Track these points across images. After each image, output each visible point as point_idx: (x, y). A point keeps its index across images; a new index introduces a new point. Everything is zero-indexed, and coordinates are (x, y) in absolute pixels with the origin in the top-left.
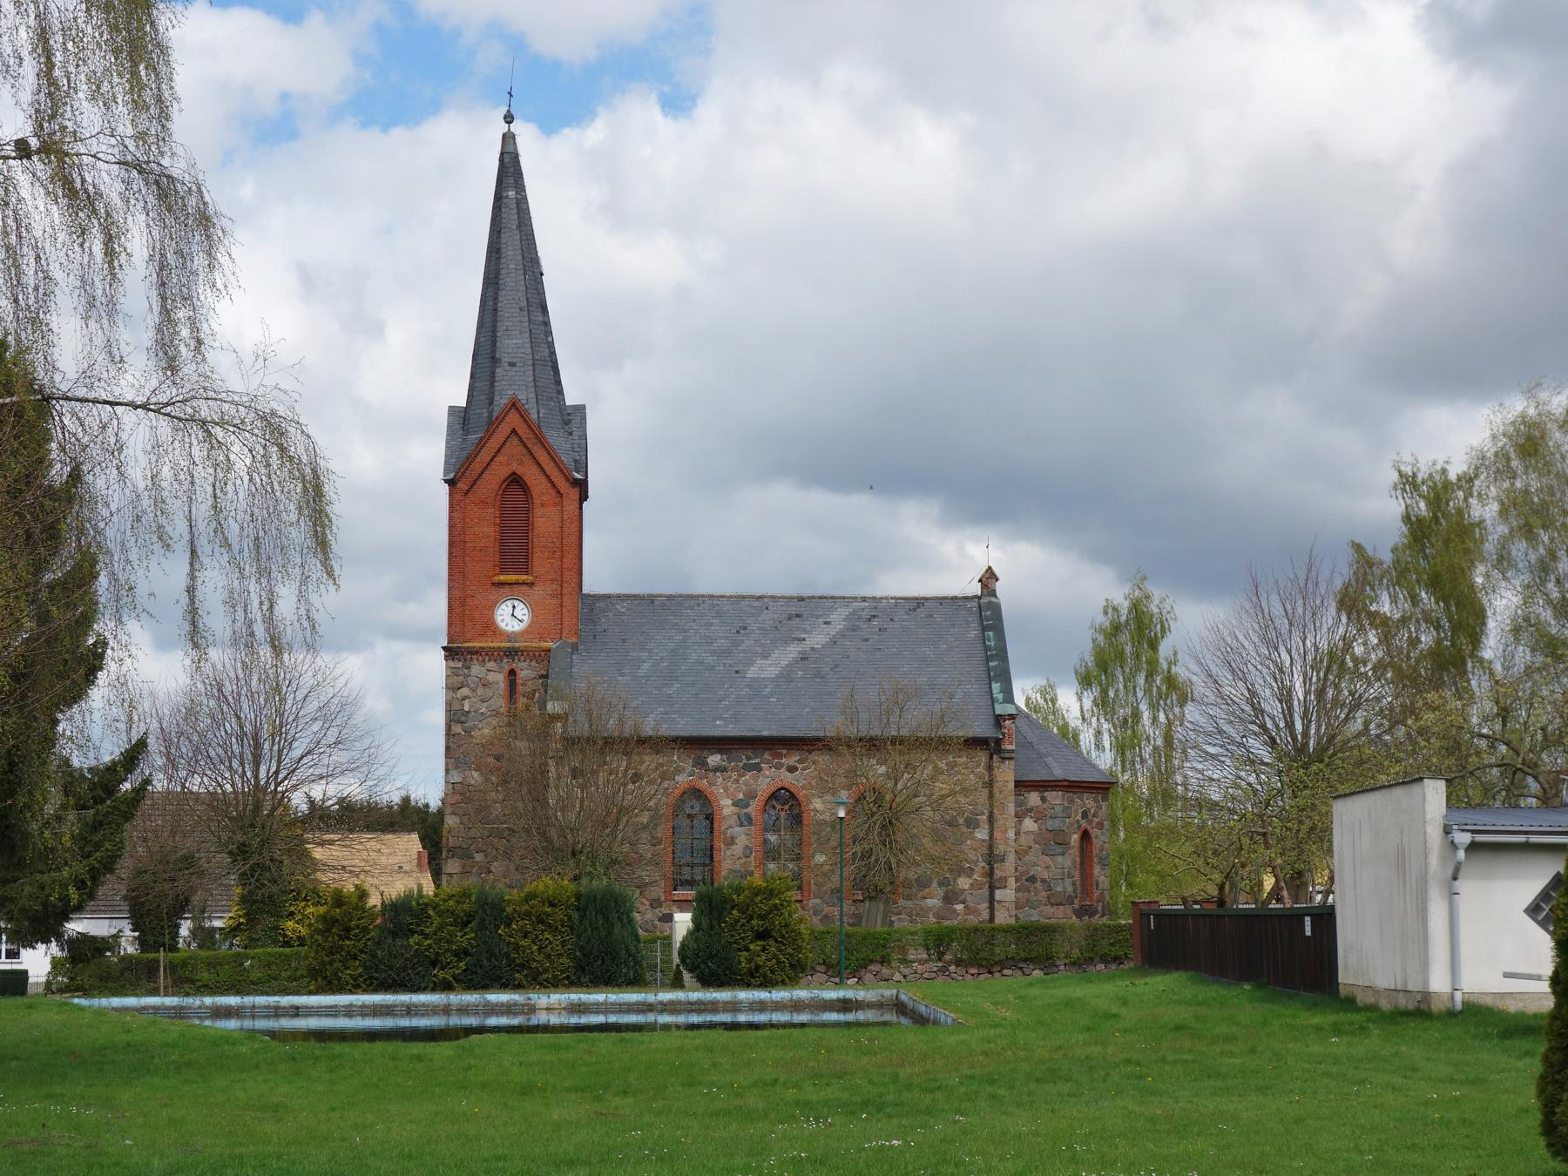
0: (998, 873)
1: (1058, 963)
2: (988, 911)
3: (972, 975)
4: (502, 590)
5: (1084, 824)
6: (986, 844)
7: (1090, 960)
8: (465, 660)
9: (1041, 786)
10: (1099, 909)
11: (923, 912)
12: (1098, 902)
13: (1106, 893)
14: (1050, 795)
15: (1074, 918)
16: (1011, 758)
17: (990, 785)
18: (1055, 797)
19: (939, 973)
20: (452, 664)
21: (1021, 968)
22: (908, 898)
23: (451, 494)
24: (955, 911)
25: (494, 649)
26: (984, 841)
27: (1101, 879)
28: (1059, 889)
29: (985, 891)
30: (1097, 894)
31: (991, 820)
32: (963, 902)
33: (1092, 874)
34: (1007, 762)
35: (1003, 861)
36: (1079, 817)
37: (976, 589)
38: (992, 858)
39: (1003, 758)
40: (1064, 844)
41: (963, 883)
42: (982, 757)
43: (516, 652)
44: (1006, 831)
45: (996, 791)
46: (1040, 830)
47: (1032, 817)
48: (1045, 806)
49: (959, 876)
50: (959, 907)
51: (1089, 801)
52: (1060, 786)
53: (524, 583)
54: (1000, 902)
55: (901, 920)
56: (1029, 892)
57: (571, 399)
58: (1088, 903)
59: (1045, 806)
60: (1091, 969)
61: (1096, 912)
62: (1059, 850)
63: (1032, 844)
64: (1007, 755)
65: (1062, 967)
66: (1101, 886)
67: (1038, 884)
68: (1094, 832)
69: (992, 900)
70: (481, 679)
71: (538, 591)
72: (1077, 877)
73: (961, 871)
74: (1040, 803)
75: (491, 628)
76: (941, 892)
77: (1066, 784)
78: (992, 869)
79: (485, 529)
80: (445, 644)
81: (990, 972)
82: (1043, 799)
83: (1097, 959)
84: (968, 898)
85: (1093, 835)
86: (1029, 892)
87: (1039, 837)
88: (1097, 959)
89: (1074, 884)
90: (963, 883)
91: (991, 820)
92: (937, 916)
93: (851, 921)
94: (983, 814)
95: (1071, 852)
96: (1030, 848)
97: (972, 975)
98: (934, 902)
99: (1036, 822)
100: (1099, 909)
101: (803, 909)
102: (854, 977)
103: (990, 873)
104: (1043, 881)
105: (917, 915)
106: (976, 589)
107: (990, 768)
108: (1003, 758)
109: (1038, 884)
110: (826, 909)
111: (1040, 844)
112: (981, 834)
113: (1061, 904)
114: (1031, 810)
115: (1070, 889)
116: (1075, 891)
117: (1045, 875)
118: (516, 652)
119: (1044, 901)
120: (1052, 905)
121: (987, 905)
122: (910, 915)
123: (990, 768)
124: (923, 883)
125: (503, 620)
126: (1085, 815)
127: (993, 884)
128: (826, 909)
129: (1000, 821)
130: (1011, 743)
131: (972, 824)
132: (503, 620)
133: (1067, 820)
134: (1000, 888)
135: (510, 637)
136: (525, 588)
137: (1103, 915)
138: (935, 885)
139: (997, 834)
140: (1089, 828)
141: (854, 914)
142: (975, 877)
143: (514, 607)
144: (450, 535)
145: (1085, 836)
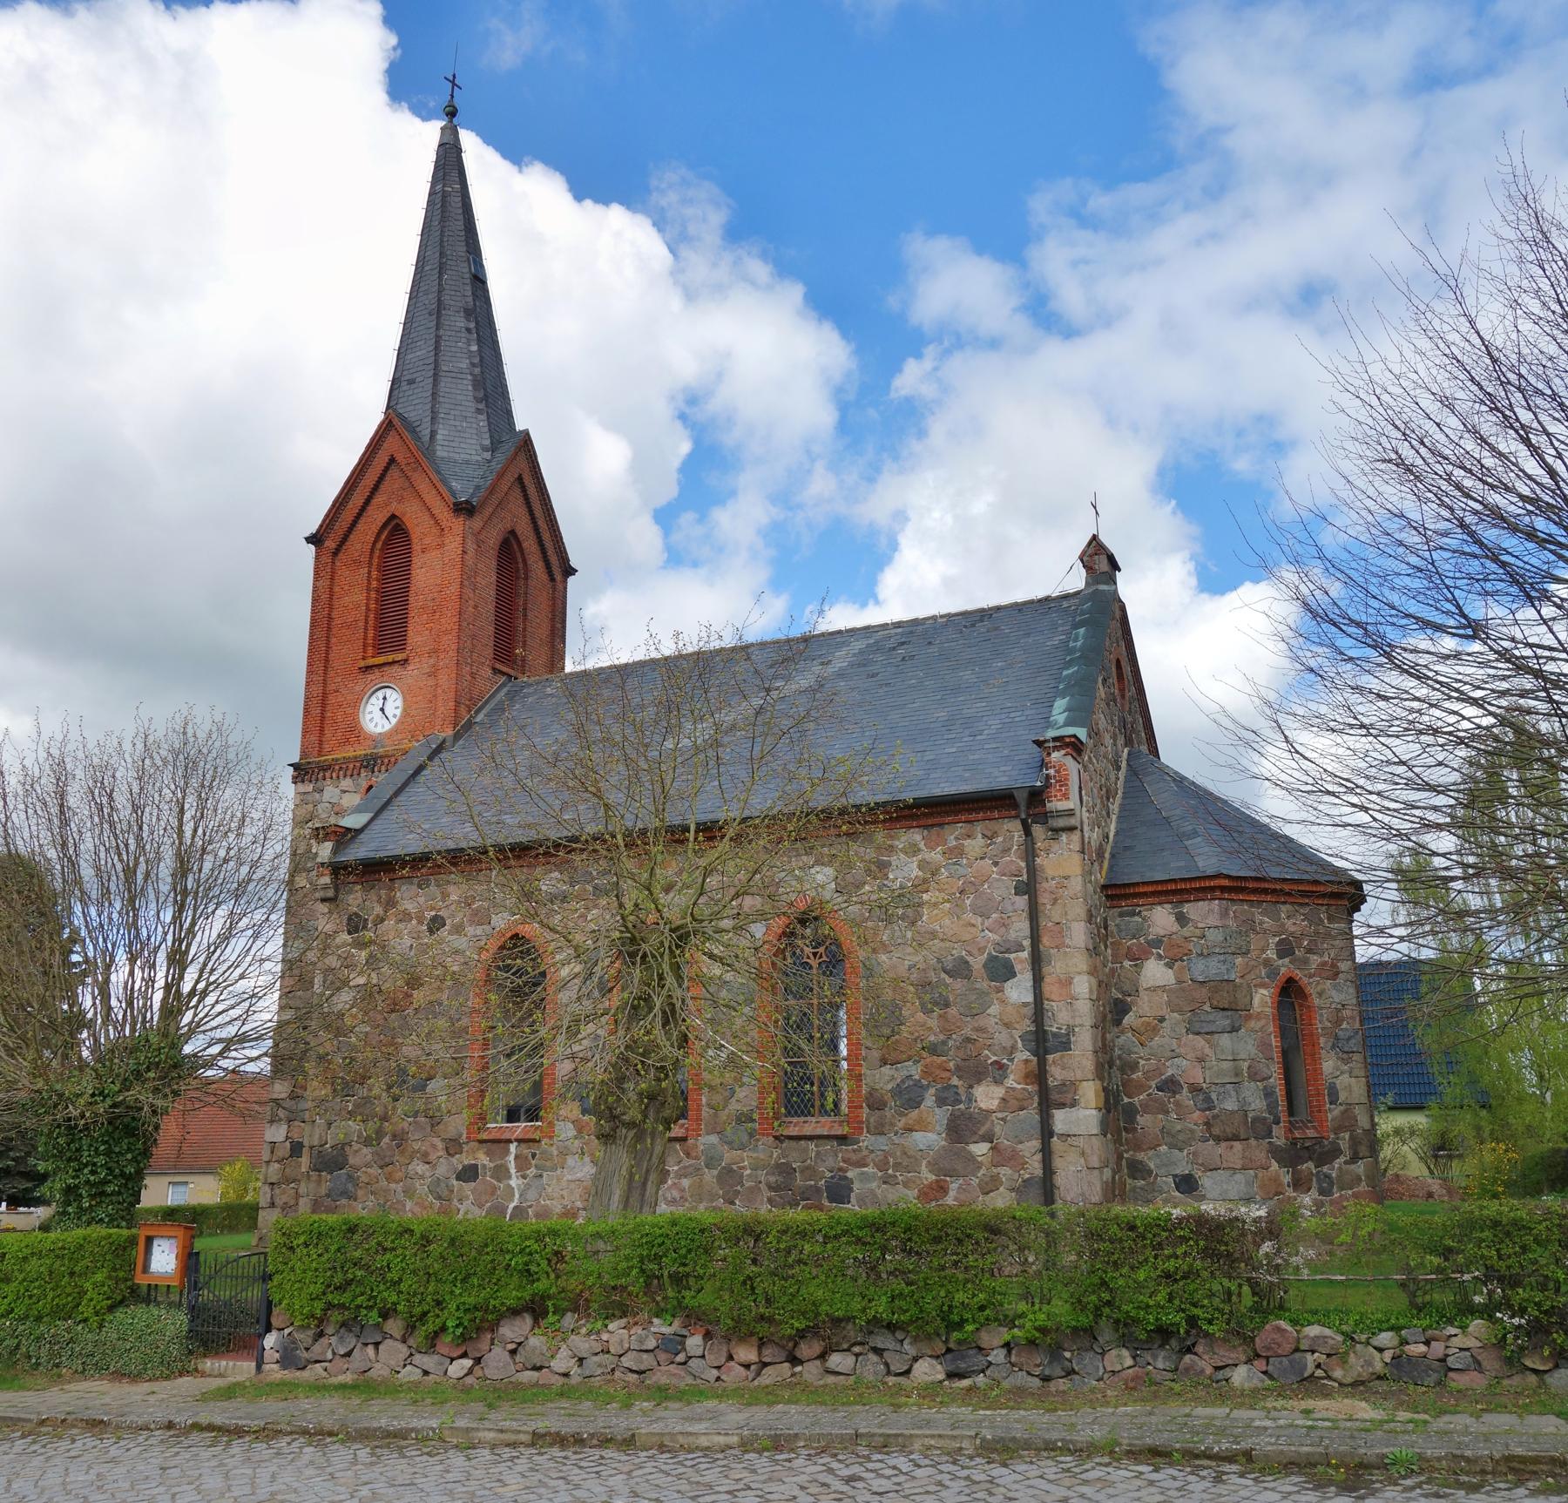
0: (1056, 1074)
1: (986, 1339)
2: (1039, 1156)
3: (747, 1366)
4: (371, 677)
5: (1285, 967)
6: (1029, 1011)
7: (1086, 1335)
8: (317, 780)
9: (1174, 892)
10: (1344, 1145)
11: (908, 1162)
12: (1337, 1130)
13: (1357, 1110)
14: (1195, 910)
15: (1275, 1165)
16: (1071, 829)
17: (1029, 887)
18: (1204, 913)
19: (662, 1357)
20: (303, 788)
21: (878, 1351)
22: (879, 1131)
23: (317, 558)
24: (971, 1158)
25: (347, 760)
26: (1025, 1005)
27: (1343, 1081)
28: (1230, 1105)
29: (1031, 1115)
30: (1334, 1113)
31: (1037, 961)
32: (988, 1138)
33: (1317, 1072)
34: (1064, 837)
35: (1065, 1045)
36: (1271, 954)
37: (1077, 581)
38: (1043, 1042)
39: (1056, 831)
40: (1233, 1010)
41: (987, 1096)
42: (1011, 830)
43: (375, 760)
44: (1069, 981)
45: (1044, 899)
46: (1179, 982)
47: (1160, 957)
48: (1186, 931)
49: (979, 1082)
50: (980, 1149)
51: (1293, 921)
52: (1212, 889)
53: (394, 662)
54: (1065, 1136)
55: (865, 1178)
56: (1167, 1112)
57: (520, 425)
58: (1311, 1133)
59: (1186, 931)
60: (1087, 1362)
61: (1336, 1152)
62: (1223, 1021)
63: (1164, 1012)
64: (1061, 823)
65: (998, 1356)
66: (1342, 1097)
67: (1184, 1096)
68: (1312, 986)
69: (1047, 1133)
70: (333, 805)
71: (414, 672)
72: (1276, 1080)
73: (976, 1072)
74: (1176, 927)
75: (354, 731)
76: (941, 1116)
77: (1226, 883)
78: (1042, 1064)
79: (355, 597)
80: (296, 760)
81: (794, 1360)
82: (1182, 919)
83: (1106, 1334)
84: (997, 1129)
85: (1312, 990)
86: (1167, 1112)
87: (1179, 996)
88: (1106, 1334)
89: (1268, 1094)
90: (987, 1096)
91: (1037, 961)
92: (934, 1166)
93: (772, 1179)
94: (1021, 948)
95: (1252, 1024)
96: (1162, 1020)
97: (747, 1366)
98: (929, 1139)
99: (1170, 966)
100: (1344, 1145)
101: (688, 1155)
102: (464, 1355)
103: (1039, 1076)
104: (1195, 1089)
105: (897, 1166)
106: (1077, 581)
107: (1030, 853)
108: (1056, 831)
109: (1184, 1096)
110: (729, 1156)
111: (1181, 1012)
112: (1019, 991)
113: (1236, 1138)
114: (1157, 943)
115: (1257, 1104)
116: (1271, 1108)
117: (1197, 1076)
118: (375, 760)
119: (1200, 1131)
120: (1218, 1139)
121: (1036, 1144)
122: (883, 1166)
123: (1030, 853)
124: (909, 1097)
125: (371, 720)
126: (1285, 950)
127: (1048, 1098)
128: (729, 1156)
129: (1055, 969)
130: (1066, 797)
131: (1001, 971)
132: (371, 720)
133: (1239, 960)
134: (1062, 1105)
135: (376, 740)
136: (396, 668)
137: (1355, 1158)
138: (929, 1100)
139: (1049, 988)
140: (1298, 974)
141: (778, 1166)
142: (1010, 1082)
143: (385, 698)
144: (313, 612)
145: (1290, 992)
